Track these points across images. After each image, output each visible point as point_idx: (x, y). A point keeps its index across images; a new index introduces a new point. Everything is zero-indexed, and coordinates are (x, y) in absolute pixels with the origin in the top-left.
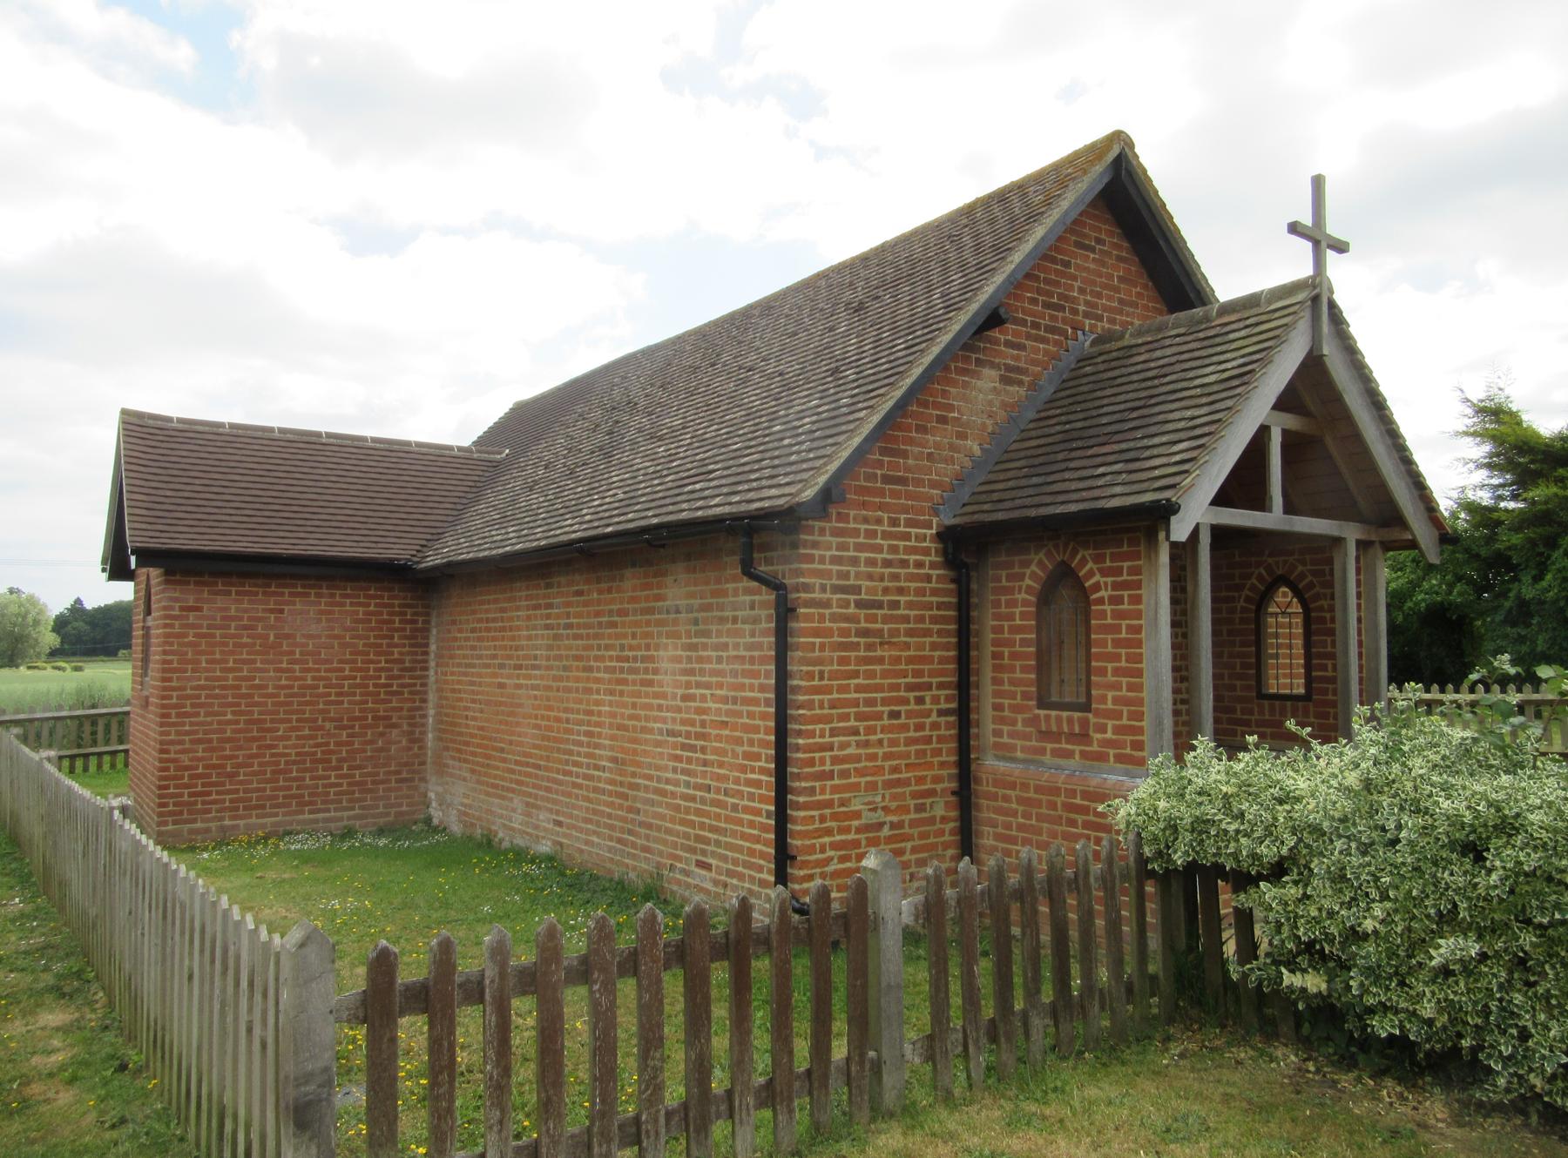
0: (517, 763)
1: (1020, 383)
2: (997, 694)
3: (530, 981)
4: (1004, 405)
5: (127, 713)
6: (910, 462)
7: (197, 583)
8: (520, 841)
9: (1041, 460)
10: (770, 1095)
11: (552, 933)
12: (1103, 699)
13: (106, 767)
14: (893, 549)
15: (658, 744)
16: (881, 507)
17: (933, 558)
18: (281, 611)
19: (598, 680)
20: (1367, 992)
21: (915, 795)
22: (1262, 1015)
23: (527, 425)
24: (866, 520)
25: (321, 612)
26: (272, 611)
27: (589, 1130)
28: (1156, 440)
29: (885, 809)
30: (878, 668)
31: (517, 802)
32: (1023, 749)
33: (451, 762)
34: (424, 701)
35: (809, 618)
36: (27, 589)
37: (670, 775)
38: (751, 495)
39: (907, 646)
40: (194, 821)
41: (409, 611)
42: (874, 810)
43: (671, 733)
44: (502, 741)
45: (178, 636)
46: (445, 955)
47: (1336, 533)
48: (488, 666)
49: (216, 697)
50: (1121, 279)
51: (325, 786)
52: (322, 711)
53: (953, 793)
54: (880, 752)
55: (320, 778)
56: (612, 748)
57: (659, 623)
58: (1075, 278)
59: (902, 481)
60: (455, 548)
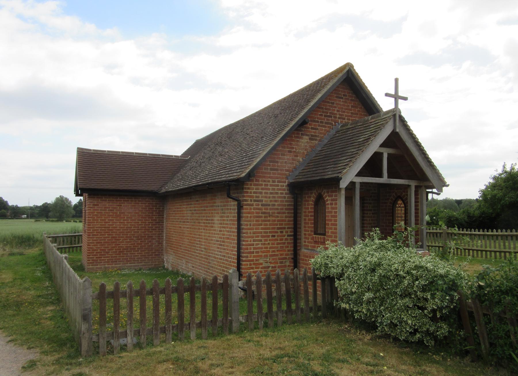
0: (184, 250)
1: (316, 140)
2: (305, 231)
3: (138, 293)
4: (311, 147)
5: (81, 235)
6: (279, 164)
7: (97, 198)
8: (184, 272)
9: (317, 163)
10: (200, 325)
11: (143, 283)
12: (328, 233)
13: (75, 251)
14: (273, 189)
15: (215, 244)
16: (270, 177)
17: (286, 192)
18: (121, 206)
19: (201, 226)
20: (354, 307)
21: (280, 259)
22: (345, 316)
23: (200, 146)
24: (265, 181)
25: (132, 206)
26: (118, 206)
27: (152, 328)
28: (343, 158)
29: (270, 262)
30: (268, 223)
31: (184, 261)
32: (311, 246)
33: (169, 250)
34: (163, 232)
35: (247, 209)
36: (65, 196)
37: (217, 253)
38: (231, 175)
39: (278, 217)
40: (97, 265)
41: (158, 205)
42: (267, 263)
43: (217, 241)
44: (180, 243)
45: (92, 213)
46: (117, 286)
47: (407, 183)
48: (177, 222)
49: (103, 230)
50: (352, 106)
51: (134, 256)
52: (132, 235)
53: (292, 259)
54: (269, 246)
55: (133, 254)
56: (204, 245)
57: (215, 210)
58: (336, 107)
59: (277, 170)
60: (170, 187)
